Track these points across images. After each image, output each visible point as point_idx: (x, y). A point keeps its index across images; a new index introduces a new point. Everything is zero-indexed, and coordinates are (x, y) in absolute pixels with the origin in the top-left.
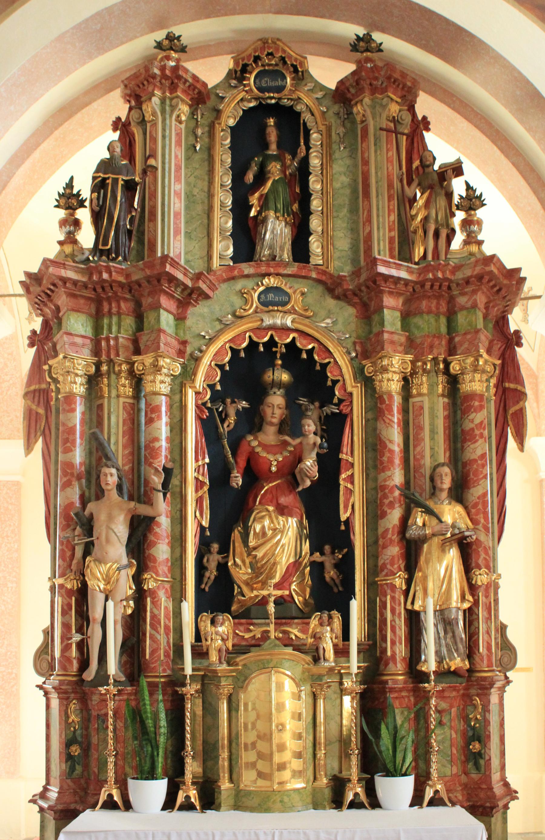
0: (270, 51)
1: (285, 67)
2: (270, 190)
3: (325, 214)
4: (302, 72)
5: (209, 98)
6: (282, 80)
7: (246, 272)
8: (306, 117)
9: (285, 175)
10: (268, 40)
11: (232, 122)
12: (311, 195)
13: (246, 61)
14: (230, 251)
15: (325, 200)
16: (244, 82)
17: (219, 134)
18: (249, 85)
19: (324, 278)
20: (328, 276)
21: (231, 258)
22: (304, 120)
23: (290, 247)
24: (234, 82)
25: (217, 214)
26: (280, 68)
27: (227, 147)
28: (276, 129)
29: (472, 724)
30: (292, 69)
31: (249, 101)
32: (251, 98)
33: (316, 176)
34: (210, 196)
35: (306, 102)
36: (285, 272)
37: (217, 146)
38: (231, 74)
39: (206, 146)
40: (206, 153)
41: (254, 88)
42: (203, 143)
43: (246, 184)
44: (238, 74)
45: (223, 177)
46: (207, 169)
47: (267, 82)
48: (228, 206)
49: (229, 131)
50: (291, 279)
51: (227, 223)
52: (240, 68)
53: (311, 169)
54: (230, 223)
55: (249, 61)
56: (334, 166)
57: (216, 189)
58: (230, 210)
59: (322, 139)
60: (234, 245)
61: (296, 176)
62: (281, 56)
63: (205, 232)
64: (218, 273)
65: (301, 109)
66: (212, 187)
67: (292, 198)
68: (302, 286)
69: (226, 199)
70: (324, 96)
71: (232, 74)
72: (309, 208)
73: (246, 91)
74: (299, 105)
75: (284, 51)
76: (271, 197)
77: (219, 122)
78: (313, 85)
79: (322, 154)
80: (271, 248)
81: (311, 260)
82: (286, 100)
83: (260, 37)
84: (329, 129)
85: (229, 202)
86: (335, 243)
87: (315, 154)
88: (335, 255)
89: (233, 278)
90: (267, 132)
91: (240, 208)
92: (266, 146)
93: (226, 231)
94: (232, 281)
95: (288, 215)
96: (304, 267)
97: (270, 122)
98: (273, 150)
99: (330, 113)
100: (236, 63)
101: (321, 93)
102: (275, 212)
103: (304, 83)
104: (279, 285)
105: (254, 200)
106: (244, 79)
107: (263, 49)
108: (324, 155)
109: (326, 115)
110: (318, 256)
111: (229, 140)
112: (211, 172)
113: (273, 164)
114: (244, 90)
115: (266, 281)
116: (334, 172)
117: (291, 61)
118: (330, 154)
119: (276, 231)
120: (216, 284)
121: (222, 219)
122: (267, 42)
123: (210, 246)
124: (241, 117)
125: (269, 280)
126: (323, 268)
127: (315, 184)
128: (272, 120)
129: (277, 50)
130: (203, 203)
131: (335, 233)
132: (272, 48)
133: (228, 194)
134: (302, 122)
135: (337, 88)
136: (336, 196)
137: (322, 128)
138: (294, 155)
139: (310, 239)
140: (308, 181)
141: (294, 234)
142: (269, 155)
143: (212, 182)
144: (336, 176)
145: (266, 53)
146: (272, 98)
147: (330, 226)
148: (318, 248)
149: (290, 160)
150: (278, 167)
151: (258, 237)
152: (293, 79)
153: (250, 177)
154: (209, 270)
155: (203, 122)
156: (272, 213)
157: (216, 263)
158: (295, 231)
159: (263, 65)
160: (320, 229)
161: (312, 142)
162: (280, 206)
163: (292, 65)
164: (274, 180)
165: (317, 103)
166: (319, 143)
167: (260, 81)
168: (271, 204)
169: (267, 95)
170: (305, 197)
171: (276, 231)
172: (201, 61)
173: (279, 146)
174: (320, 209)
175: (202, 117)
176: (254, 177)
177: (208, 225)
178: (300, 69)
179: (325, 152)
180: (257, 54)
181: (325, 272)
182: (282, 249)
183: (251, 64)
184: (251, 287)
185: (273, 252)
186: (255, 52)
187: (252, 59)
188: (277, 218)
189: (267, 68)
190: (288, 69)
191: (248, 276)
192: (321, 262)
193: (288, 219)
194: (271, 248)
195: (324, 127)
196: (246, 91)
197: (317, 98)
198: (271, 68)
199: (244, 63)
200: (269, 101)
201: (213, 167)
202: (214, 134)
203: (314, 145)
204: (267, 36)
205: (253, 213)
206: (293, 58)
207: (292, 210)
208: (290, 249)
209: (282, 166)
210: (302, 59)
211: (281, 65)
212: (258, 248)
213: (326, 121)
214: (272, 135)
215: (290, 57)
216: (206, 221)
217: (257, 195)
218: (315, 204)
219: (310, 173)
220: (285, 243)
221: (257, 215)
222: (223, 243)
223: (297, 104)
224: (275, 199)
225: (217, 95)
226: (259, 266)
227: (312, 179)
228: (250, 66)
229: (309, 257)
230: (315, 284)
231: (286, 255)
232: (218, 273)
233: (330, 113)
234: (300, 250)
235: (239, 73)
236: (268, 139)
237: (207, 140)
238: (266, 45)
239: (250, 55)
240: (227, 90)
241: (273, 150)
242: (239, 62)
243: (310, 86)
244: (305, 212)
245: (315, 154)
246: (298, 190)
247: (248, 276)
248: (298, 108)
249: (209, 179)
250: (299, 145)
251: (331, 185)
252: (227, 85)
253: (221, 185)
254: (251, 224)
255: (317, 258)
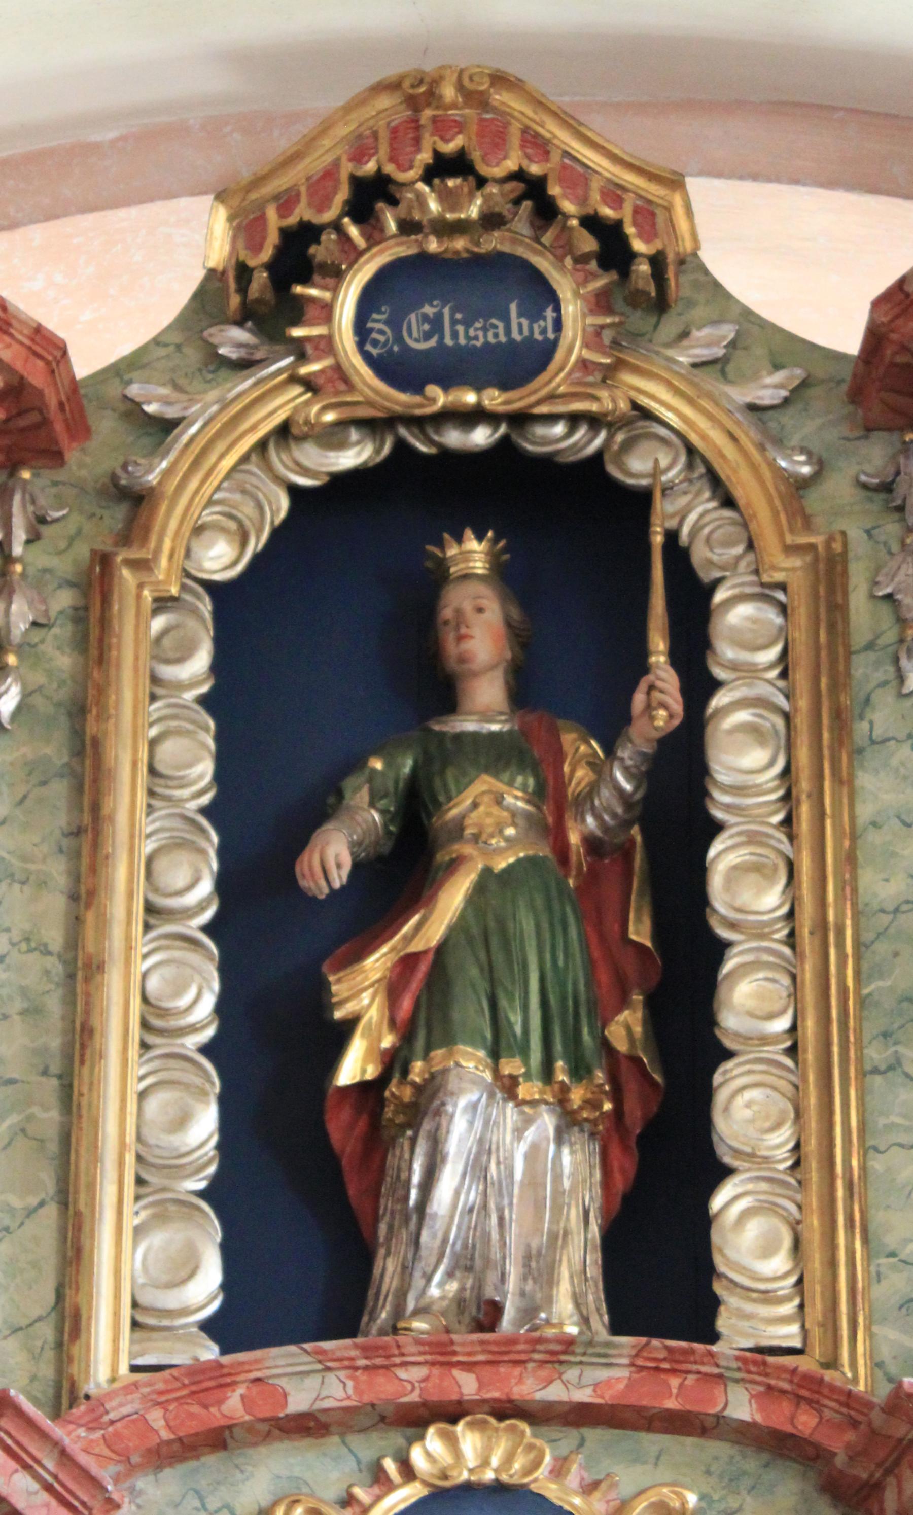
0: (449, 148)
1: (548, 238)
2: (453, 930)
3: (810, 1055)
4: (657, 262)
5: (80, 429)
6: (535, 315)
7: (300, 1400)
8: (686, 513)
9: (562, 851)
10: (436, 81)
11: (220, 559)
12: (720, 948)
13: (303, 212)
14: (205, 1287)
15: (808, 974)
16: (297, 332)
17: (141, 625)
18: (327, 345)
19: (806, 1422)
20: (832, 1410)
21: (210, 1327)
22: (672, 536)
23: (594, 1259)
24: (234, 339)
25: (119, 1069)
26: (516, 239)
27: (189, 696)
28: (504, 600)
29: (378, 764)
30: (588, 243)
31: (332, 436)
32: (342, 424)
33: (753, 839)
34: (80, 969)
35: (674, 426)
36: (555, 1393)
37: (127, 690)
38: (210, 301)
39: (63, 694)
40: (61, 734)
41: (357, 361)
42: (38, 678)
43: (311, 900)
44: (267, 291)
45: (161, 865)
46: (62, 820)
47: (436, 324)
48: (194, 1029)
49: (206, 606)
50: (594, 1435)
51: (182, 1121)
52: (267, 254)
53: (720, 804)
54: (205, 1123)
55: (322, 205)
56: (865, 780)
57: (117, 932)
58: (206, 1050)
59: (784, 634)
60: (228, 1251)
61: (627, 853)
62: (519, 175)
63: (48, 1181)
64: (117, 1409)
65: (656, 472)
66: (90, 917)
67: (604, 977)
68: (664, 1473)
69: (179, 990)
70: (796, 396)
71: (224, 293)
72: (710, 1021)
73: (309, 384)
74: (645, 446)
75: (537, 144)
76: (469, 973)
77: (135, 554)
78: (728, 331)
79: (787, 717)
80: (467, 1262)
81: (723, 1323)
82: (559, 429)
83: (390, 71)
84: (830, 571)
85: (200, 1002)
86: (878, 1217)
87: (743, 716)
88: (878, 1291)
89: (218, 1440)
90: (447, 613)
91: (271, 1044)
92: (441, 690)
93: (178, 1171)
94: (211, 1460)
95: (579, 1070)
96: (676, 1365)
97: (466, 556)
98: (485, 706)
99: (839, 487)
100: (247, 227)
101: (779, 377)
102: (495, 1054)
103: (670, 326)
104: (514, 1473)
105: (362, 992)
106: (296, 310)
107: (407, 134)
108: (802, 722)
109: (813, 501)
110: (768, 1297)
111: (200, 661)
112: (87, 834)
113: (484, 784)
114: (294, 379)
115: (430, 1451)
116: (865, 811)
117: (583, 201)
118: (838, 715)
119: (501, 1169)
120: (105, 1474)
121: (153, 1104)
122: (432, 97)
123: (73, 1255)
124: (276, 533)
125: (452, 1441)
126: (804, 1364)
127: (742, 886)
128: (472, 544)
129: (495, 136)
130: (33, 1011)
131: (877, 1164)
132: (460, 127)
133: (194, 958)
134: (658, 540)
135: (874, 338)
136: (882, 948)
137: (787, 568)
138: (610, 725)
139: (717, 1202)
140: (698, 872)
141: (620, 1185)
142: (459, 737)
143: (92, 894)
144: (873, 838)
145: (425, 157)
146: (472, 417)
147: (847, 1117)
148: (767, 1250)
149: (593, 764)
150: (516, 800)
151: (386, 1204)
152: (601, 303)
153: (332, 858)
154: (66, 1395)
155: (40, 558)
156: (470, 1063)
157: (107, 1356)
158: (626, 1166)
159: (408, 227)
160: (779, 1142)
161: (726, 650)
162: (524, 1018)
163: (591, 222)
164: (487, 871)
165: (749, 436)
166: (774, 652)
167: (395, 323)
168: (470, 1009)
169: (440, 398)
170: (684, 969)
171: (501, 1169)
172: (37, 233)
173: (523, 690)
174: (783, 1024)
175: (33, 539)
176: (357, 867)
177: (66, 1140)
178: (638, 246)
179: (803, 703)
180: (371, 167)
181: (813, 1383)
182: (540, 1268)
183: (337, 226)
184: (333, 1492)
185: (479, 1286)
186: (359, 157)
187: (343, 195)
188: (508, 1087)
189: (433, 245)
190: (564, 248)
191: (309, 1426)
192: (788, 1334)
193: (577, 1096)
194: (467, 1262)
195: (796, 562)
196: (309, 384)
197: (753, 408)
198: (460, 244)
199: (292, 220)
200: (453, 438)
201: (96, 808)
202: (104, 623)
203: (734, 666)
204: (429, 66)
205: (354, 1067)
206: (595, 185)
207: (605, 1045)
208: (594, 1271)
209: (538, 796)
210: (655, 191)
211: (522, 221)
212: (388, 1268)
213: (808, 524)
214: (480, 629)
215: (578, 176)
216: (49, 1117)
217: (377, 963)
218: (749, 1000)
219: (715, 828)
220: (558, 1239)
221: (381, 1082)
222: (157, 1239)
223: (628, 446)
224: (493, 982)
225: (133, 412)
226: (382, 1362)
227: (724, 857)
228: (329, 238)
229: (714, 1303)
230: (751, 1463)
231: (571, 1301)
232: (117, 1409)
233: (839, 487)
234: (658, 1264)
235: (261, 278)
236: (451, 648)
237: (65, 661)
238: (427, 114)
239: (330, 174)
240: (197, 384)
241: (485, 706)
242: (261, 219)
243: (709, 340)
244: (689, 1045)
245: (743, 716)
246: (640, 932)
247: (309, 1426)
248: (637, 467)
249: (76, 878)
250: (644, 668)
251: (850, 887)
252: (193, 355)
253: (150, 909)
254: (342, 1130)
255: (765, 1311)
